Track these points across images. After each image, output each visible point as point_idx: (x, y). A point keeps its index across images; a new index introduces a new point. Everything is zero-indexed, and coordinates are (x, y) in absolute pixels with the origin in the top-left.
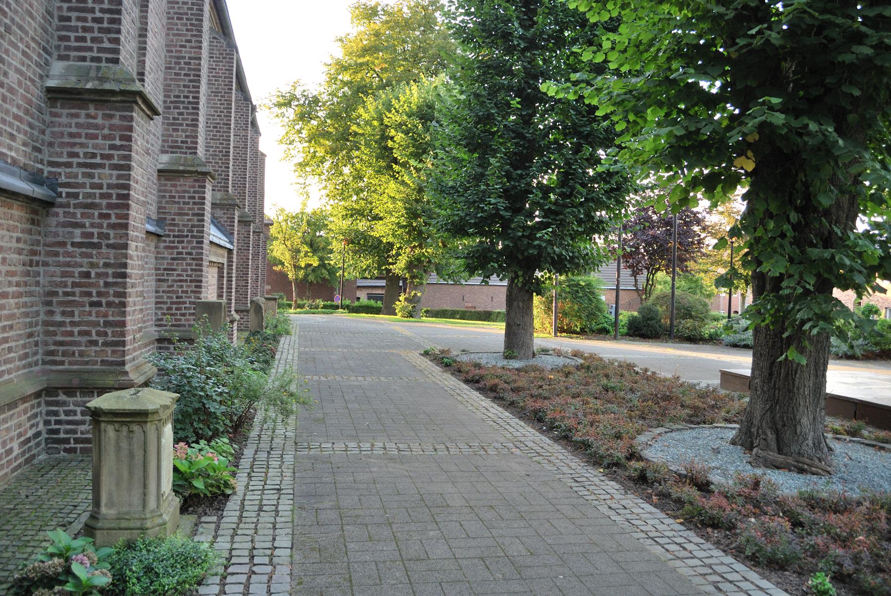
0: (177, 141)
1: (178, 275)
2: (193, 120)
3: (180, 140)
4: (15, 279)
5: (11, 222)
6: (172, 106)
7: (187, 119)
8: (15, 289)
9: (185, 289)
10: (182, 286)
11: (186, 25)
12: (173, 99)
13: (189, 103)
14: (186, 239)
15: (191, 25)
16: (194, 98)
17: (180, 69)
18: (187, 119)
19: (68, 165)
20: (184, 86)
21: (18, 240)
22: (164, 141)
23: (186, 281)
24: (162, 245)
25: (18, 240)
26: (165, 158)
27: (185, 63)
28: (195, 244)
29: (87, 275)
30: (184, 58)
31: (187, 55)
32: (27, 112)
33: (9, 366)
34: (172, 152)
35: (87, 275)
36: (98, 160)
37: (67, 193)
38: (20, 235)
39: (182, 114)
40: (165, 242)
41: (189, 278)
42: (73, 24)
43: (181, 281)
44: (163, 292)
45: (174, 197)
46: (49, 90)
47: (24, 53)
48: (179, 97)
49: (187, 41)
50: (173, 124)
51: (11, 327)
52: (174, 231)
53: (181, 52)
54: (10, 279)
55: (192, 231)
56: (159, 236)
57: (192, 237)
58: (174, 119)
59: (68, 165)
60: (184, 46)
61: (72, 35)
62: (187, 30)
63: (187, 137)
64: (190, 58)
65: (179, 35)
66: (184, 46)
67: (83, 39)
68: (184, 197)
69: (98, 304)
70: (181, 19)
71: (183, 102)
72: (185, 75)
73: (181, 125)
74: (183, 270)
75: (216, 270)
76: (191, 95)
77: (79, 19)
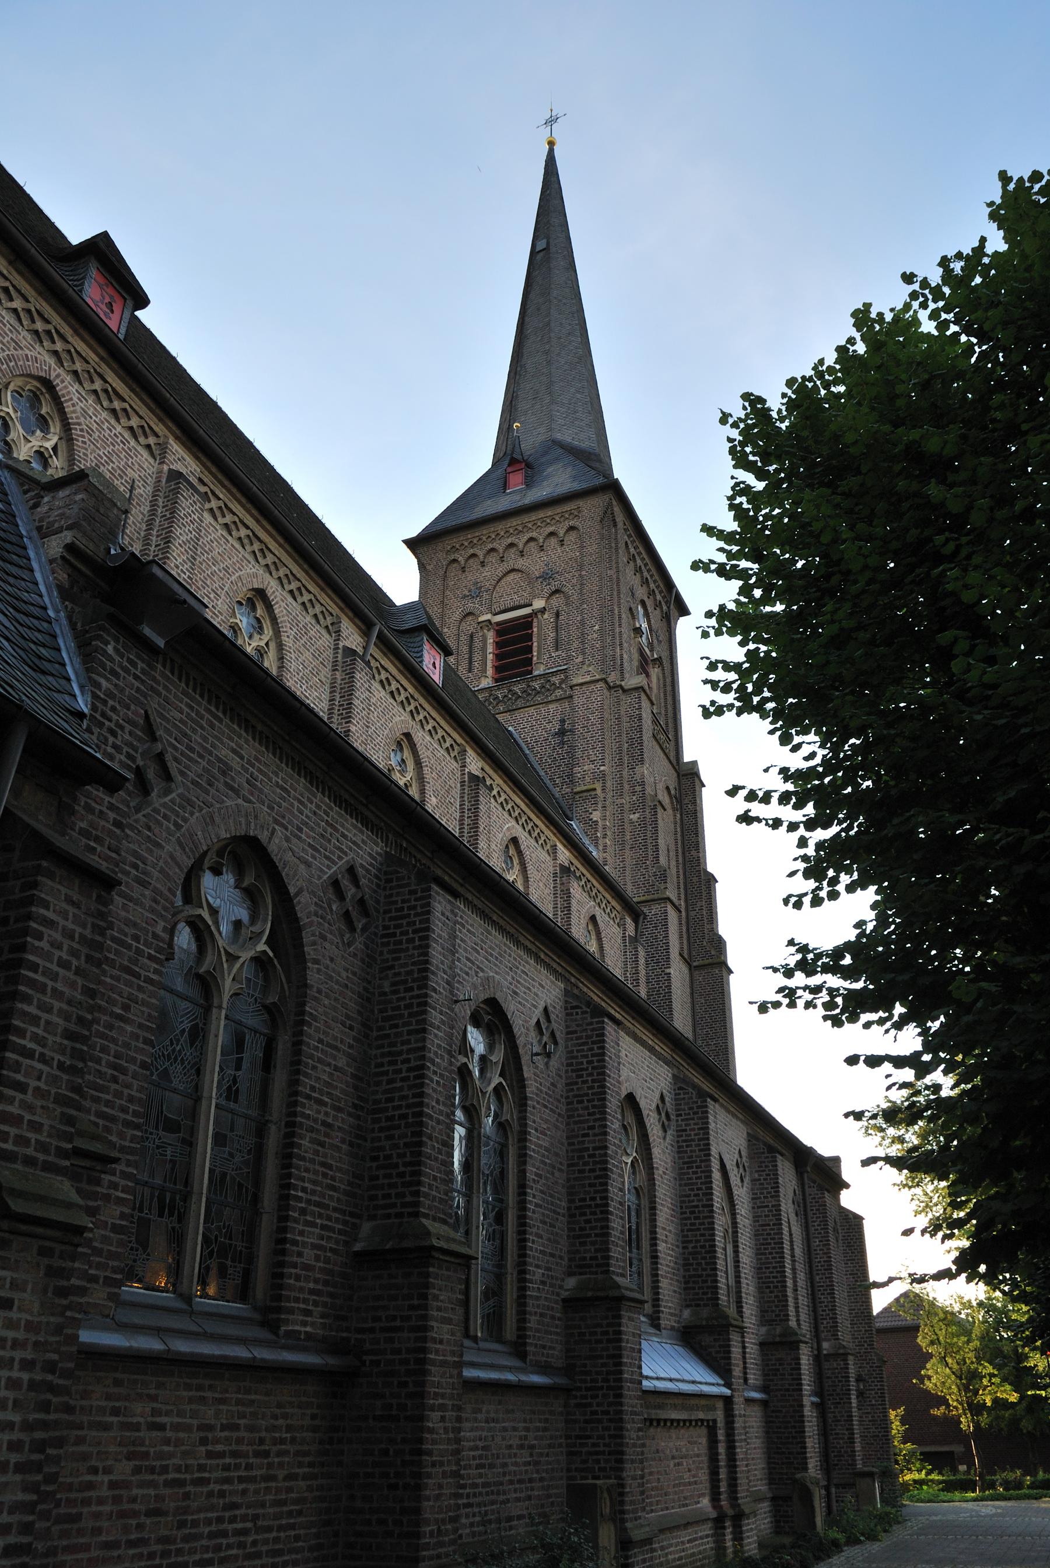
0: (585, 1258)
1: (594, 1445)
2: (602, 1228)
3: (588, 1255)
4: (307, 1459)
5: (304, 1399)
6: (577, 1212)
7: (596, 1228)
8: (306, 1470)
9: (603, 1465)
10: (598, 1462)
11: (587, 1108)
12: (578, 1204)
13: (597, 1206)
14: (600, 1393)
15: (594, 1107)
16: (601, 1198)
17: (585, 1164)
18: (596, 1228)
19: (372, 1330)
20: (590, 1185)
21: (314, 1417)
22: (570, 1260)
23: (603, 1453)
24: (573, 1402)
25: (314, 1417)
26: (571, 1282)
27: (590, 1156)
28: (611, 1399)
29: (385, 1452)
30: (588, 1149)
31: (591, 1145)
32: (326, 1283)
33: (294, 1556)
34: (581, 1274)
35: (385, 1452)
36: (398, 1323)
37: (371, 1361)
38: (315, 1411)
39: (588, 1221)
40: (576, 1397)
41: (607, 1449)
42: (380, 1182)
43: (597, 1453)
44: (576, 1470)
45: (584, 1334)
46: (357, 1254)
47: (323, 1227)
48: (584, 1200)
49: (589, 1128)
50: (579, 1237)
51: (300, 1513)
52: (585, 1381)
53: (583, 1142)
54: (300, 1459)
55: (608, 1381)
56: (568, 1390)
57: (609, 1388)
58: (581, 1229)
59: (372, 1330)
60: (587, 1135)
61: (380, 1193)
62: (589, 1114)
63: (596, 1251)
64: (594, 1149)
65: (580, 1122)
66: (587, 1135)
67: (389, 1196)
68: (596, 1333)
69: (393, 1487)
70: (582, 1102)
71: (590, 1206)
72: (590, 1171)
73: (589, 1236)
74: (600, 1437)
75: (704, 1431)
76: (598, 1196)
77: (386, 1176)
